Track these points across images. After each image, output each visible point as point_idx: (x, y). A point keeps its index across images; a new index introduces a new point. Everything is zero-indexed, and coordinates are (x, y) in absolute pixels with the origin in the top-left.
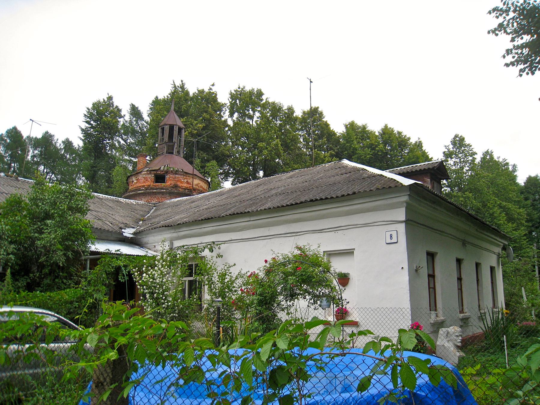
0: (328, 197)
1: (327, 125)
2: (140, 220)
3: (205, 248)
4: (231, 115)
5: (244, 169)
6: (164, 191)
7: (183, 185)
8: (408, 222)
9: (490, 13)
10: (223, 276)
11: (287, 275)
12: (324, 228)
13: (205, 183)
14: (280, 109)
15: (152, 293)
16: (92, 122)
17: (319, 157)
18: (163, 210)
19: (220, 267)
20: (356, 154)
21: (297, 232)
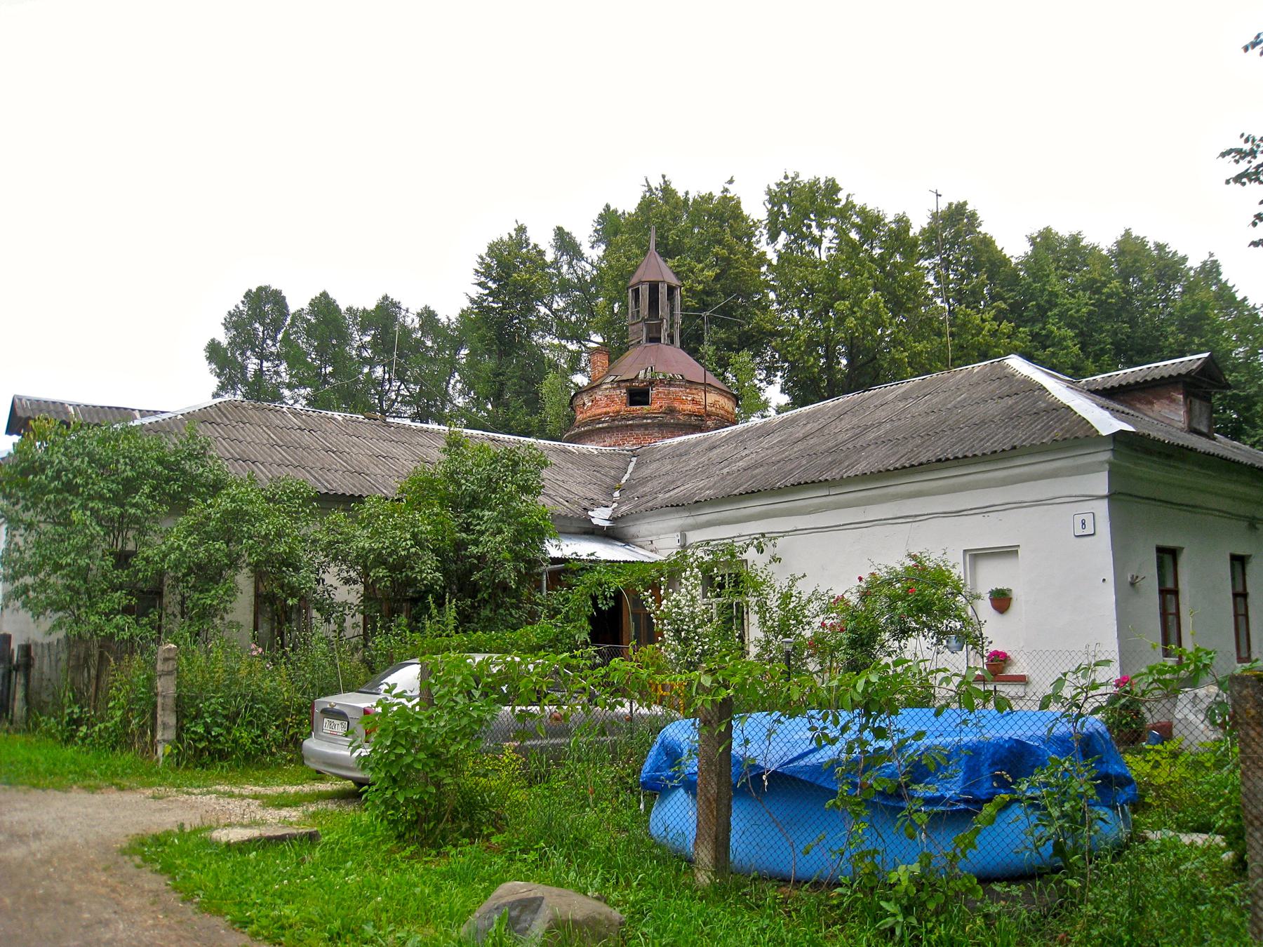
0: (967, 454)
1: (987, 242)
2: (615, 489)
3: (748, 546)
4: (773, 238)
5: (808, 361)
6: (649, 421)
7: (685, 407)
8: (1112, 497)
9: (1223, 155)
10: (786, 597)
11: (893, 599)
12: (963, 508)
13: (729, 398)
14: (879, 222)
15: (678, 631)
16: (490, 284)
17: (969, 322)
18: (654, 465)
19: (781, 582)
20: (1056, 305)
21: (916, 516)
